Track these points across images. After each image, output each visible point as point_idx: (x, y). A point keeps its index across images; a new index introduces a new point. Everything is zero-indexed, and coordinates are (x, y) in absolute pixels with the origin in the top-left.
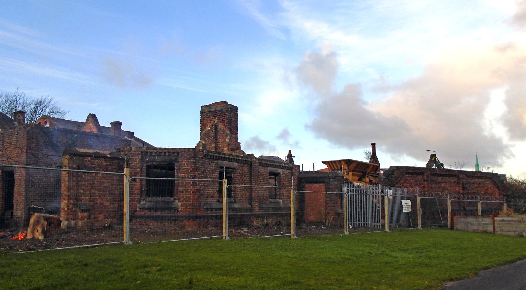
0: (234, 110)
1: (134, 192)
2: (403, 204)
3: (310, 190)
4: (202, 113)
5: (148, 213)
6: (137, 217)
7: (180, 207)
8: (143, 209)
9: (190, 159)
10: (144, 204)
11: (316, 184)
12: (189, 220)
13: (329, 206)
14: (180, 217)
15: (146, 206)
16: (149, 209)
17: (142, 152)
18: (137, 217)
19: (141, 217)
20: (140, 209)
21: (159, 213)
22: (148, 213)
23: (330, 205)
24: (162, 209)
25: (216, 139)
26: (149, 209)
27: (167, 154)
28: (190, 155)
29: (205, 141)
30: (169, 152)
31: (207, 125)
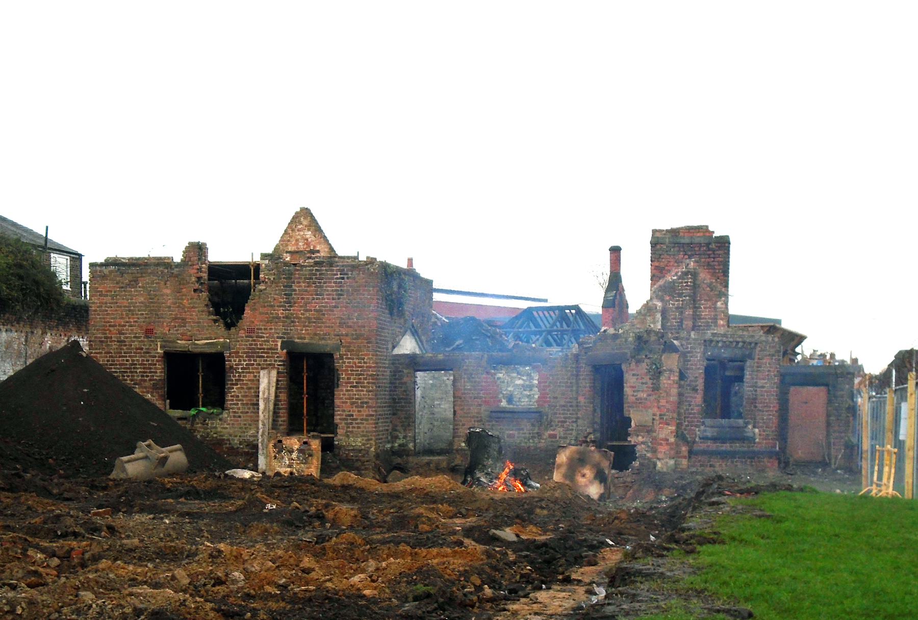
0: (724, 243)
1: (692, 409)
2: (418, 380)
3: (800, 395)
4: (654, 244)
5: (713, 446)
6: (697, 453)
7: (757, 436)
8: (704, 439)
9: (773, 355)
10: (705, 431)
11: (810, 388)
12: (771, 458)
13: (835, 431)
14: (759, 453)
15: (709, 434)
16: (714, 439)
17: (705, 341)
18: (697, 453)
19: (704, 452)
20: (700, 438)
21: (726, 447)
22: (713, 446)
23: (836, 428)
24: (733, 440)
25: (694, 299)
26: (714, 439)
27: (740, 344)
28: (773, 347)
29: (662, 300)
30: (744, 342)
31: (669, 271)
